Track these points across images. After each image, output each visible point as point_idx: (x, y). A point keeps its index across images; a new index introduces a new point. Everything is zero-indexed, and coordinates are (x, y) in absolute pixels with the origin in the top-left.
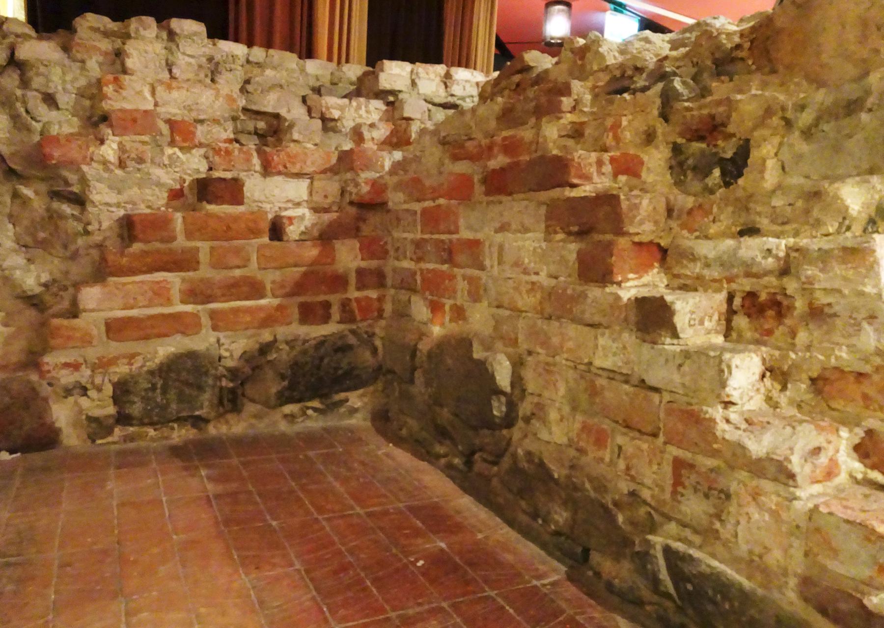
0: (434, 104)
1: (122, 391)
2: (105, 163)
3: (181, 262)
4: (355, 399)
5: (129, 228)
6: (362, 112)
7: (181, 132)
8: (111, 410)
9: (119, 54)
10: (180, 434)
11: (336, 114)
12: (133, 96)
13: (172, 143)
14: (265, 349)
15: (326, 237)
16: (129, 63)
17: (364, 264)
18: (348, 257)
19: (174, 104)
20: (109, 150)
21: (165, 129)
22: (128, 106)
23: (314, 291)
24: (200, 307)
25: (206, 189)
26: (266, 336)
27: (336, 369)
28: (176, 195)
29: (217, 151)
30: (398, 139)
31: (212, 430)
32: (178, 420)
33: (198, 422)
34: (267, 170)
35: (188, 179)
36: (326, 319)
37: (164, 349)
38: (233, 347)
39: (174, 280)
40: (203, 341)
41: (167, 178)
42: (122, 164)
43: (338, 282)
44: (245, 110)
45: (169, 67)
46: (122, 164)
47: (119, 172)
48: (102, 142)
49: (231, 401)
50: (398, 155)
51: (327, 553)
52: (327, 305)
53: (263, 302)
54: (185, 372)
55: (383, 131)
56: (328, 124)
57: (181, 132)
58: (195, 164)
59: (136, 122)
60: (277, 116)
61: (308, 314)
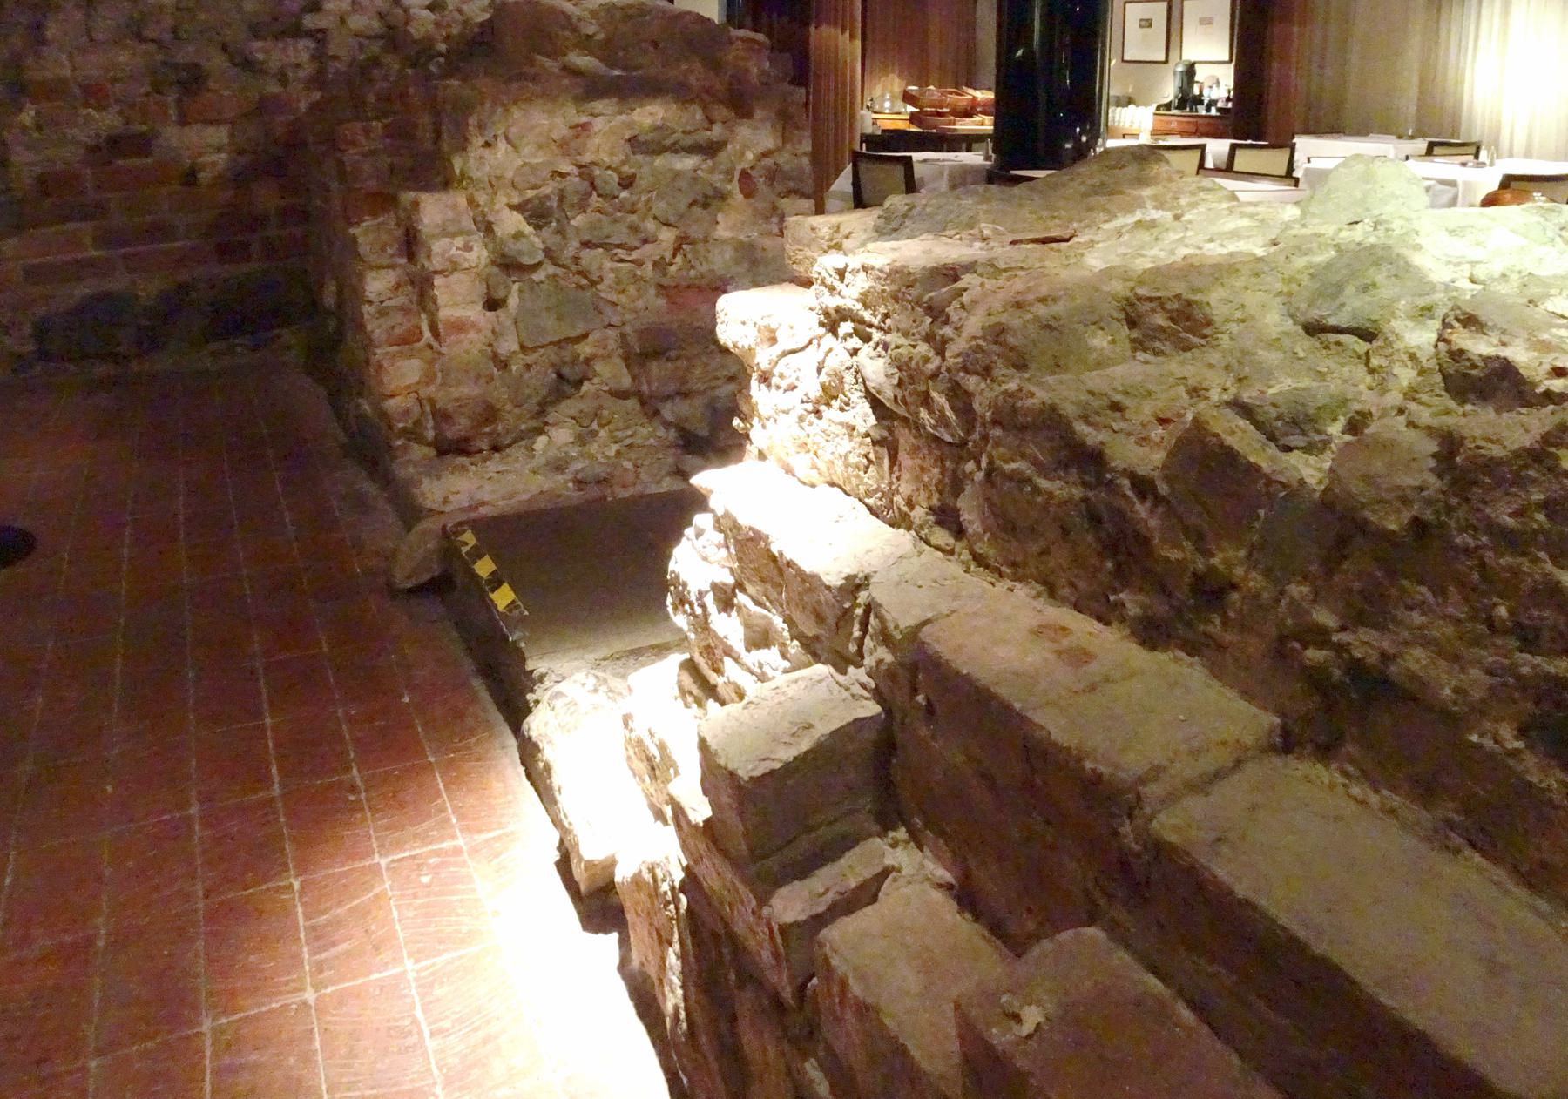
0: (368, 37)
1: (41, 332)
2: (24, 129)
3: (100, 210)
4: (288, 336)
5: (46, 184)
6: (291, 51)
7: (94, 94)
8: (31, 347)
9: (39, 26)
10: (101, 369)
11: (260, 56)
12: (56, 64)
13: (87, 105)
14: (183, 289)
15: (240, 179)
16: (49, 34)
17: (283, 203)
18: (267, 198)
19: (93, 67)
20: (28, 116)
21: (77, 91)
22: (49, 75)
23: (231, 233)
24: (112, 252)
25: (116, 144)
26: (184, 276)
27: (608, 237)
28: (93, 149)
29: (132, 106)
30: (318, 80)
31: (135, 366)
32: (97, 356)
33: (116, 358)
34: (183, 121)
35: (104, 135)
36: (248, 258)
37: (82, 290)
38: (150, 288)
39: (86, 229)
40: (118, 283)
41: (83, 135)
42: (39, 128)
43: (256, 222)
44: (165, 63)
45: (88, 31)
46: (39, 128)
47: (36, 135)
48: (21, 110)
49: (150, 342)
50: (317, 95)
51: (1235, 234)
52: (245, 245)
53: (177, 244)
54: (102, 313)
55: (308, 70)
56: (248, 65)
57: (94, 94)
58: (108, 120)
59: (53, 90)
60: (196, 66)
61: (225, 252)
